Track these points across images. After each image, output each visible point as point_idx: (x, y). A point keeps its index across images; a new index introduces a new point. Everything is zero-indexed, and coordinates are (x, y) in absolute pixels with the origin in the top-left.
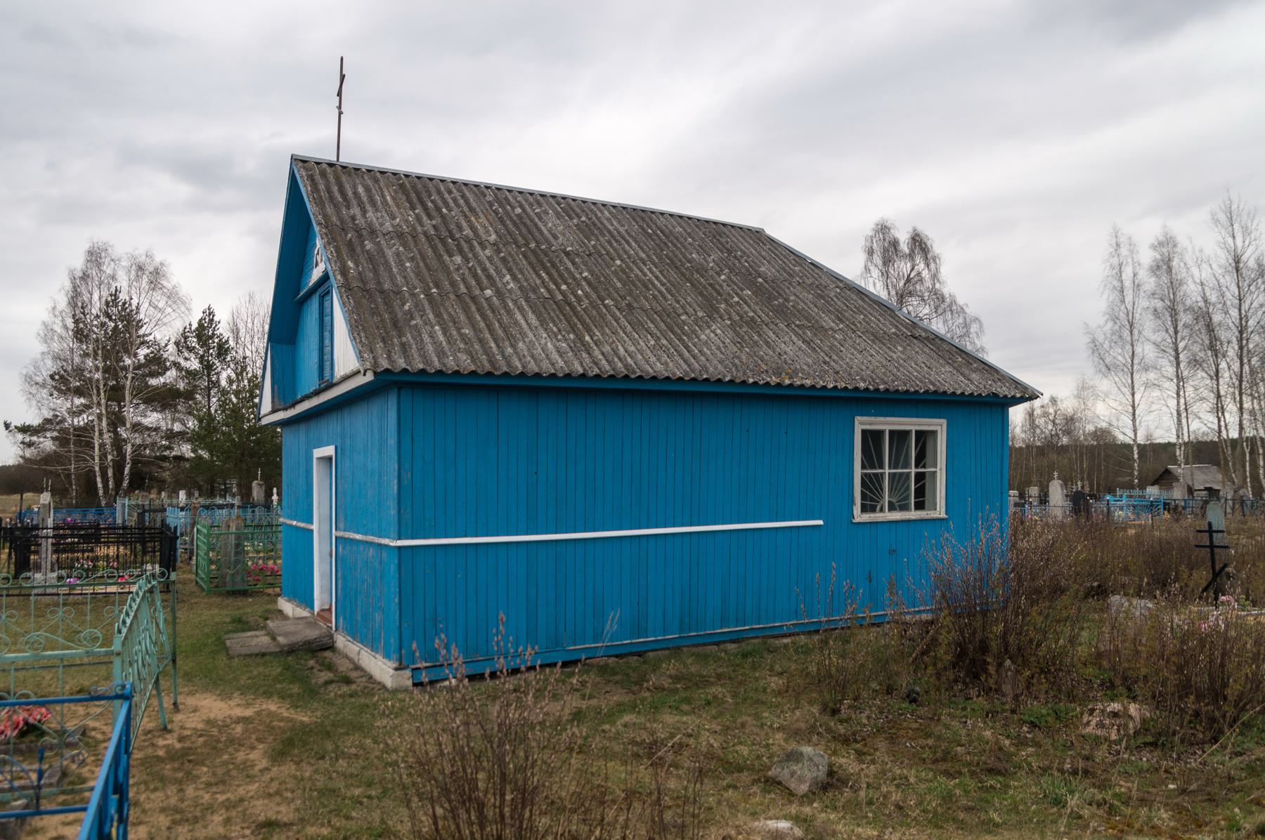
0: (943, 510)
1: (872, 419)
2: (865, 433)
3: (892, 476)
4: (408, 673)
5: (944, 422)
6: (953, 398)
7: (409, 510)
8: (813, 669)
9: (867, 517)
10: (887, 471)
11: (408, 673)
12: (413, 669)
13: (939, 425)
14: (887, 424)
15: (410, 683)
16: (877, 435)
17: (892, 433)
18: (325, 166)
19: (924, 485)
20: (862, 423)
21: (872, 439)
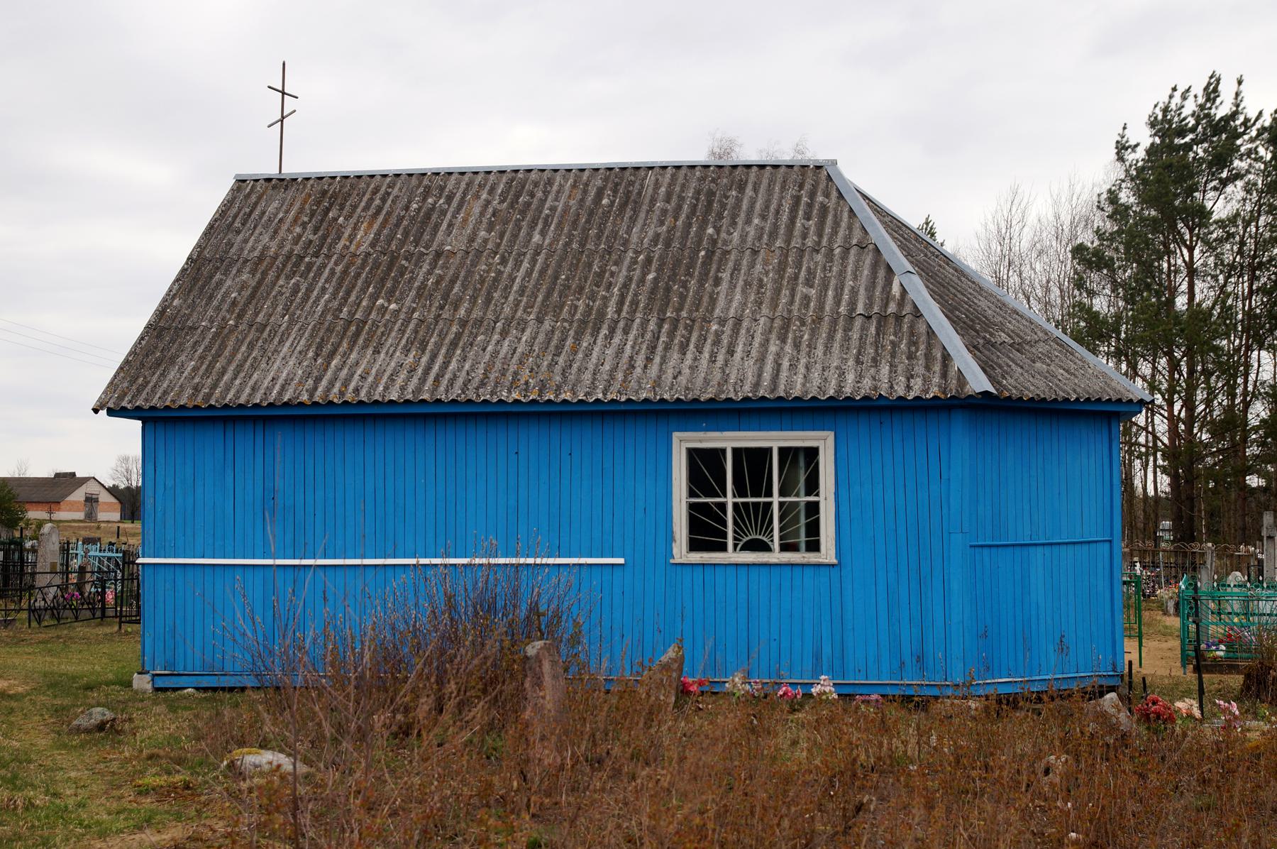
0: (833, 552)
1: (701, 434)
2: (693, 454)
3: (781, 504)
4: (148, 677)
5: (830, 435)
6: (1019, 404)
7: (151, 532)
8: (1154, 481)
9: (697, 557)
10: (776, 499)
11: (148, 677)
12: (154, 675)
13: (823, 441)
14: (728, 440)
15: (149, 686)
16: (715, 456)
17: (783, 451)
18: (922, 328)
19: (818, 520)
20: (683, 442)
21: (705, 468)
